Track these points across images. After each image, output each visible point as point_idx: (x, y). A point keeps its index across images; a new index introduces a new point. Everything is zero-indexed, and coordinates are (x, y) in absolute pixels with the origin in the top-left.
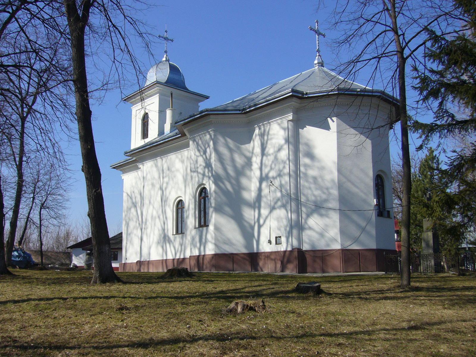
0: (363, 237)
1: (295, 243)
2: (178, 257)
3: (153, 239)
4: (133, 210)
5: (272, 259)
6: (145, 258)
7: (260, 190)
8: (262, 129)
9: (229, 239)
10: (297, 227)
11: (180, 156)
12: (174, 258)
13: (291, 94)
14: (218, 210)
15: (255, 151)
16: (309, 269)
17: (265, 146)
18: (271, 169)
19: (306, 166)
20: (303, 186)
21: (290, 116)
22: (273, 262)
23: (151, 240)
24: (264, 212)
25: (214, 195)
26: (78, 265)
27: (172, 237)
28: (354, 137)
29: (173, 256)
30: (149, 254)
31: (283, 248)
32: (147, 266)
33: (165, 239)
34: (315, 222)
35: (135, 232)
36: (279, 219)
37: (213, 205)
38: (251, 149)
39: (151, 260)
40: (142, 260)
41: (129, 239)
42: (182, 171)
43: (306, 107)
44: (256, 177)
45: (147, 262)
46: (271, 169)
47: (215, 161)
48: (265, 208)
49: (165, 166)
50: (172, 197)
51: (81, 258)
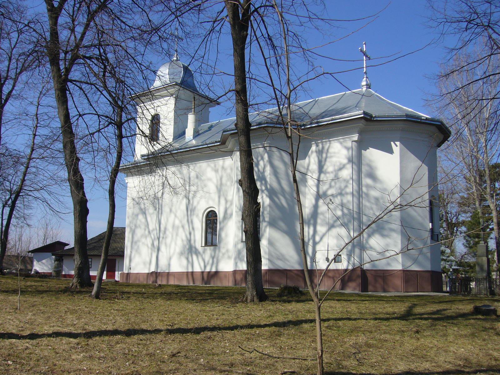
0: (421, 258)
1: (357, 264)
2: (208, 269)
3: (175, 250)
4: (141, 217)
5: (330, 277)
6: (163, 268)
7: (316, 207)
8: (320, 146)
9: (282, 255)
10: (357, 245)
11: (212, 165)
12: (203, 270)
13: (362, 116)
14: (273, 224)
15: (310, 168)
16: (370, 288)
17: (323, 163)
18: (331, 187)
19: (368, 186)
20: (365, 206)
21: (356, 137)
22: (332, 280)
23: (172, 251)
24: (321, 229)
25: (268, 209)
26: (40, 271)
27: (200, 249)
28: (414, 162)
29: (201, 268)
30: (169, 265)
31: (343, 265)
32: (166, 277)
33: (190, 250)
34: (376, 242)
35: (143, 240)
36: (339, 236)
37: (267, 219)
38: (306, 166)
39: (171, 271)
40: (159, 271)
41: (135, 247)
42: (215, 180)
43: (373, 129)
44: (311, 193)
45: (166, 274)
46: (331, 187)
47: (270, 174)
48: (322, 225)
49: (193, 174)
50: (202, 206)
51: (44, 264)
